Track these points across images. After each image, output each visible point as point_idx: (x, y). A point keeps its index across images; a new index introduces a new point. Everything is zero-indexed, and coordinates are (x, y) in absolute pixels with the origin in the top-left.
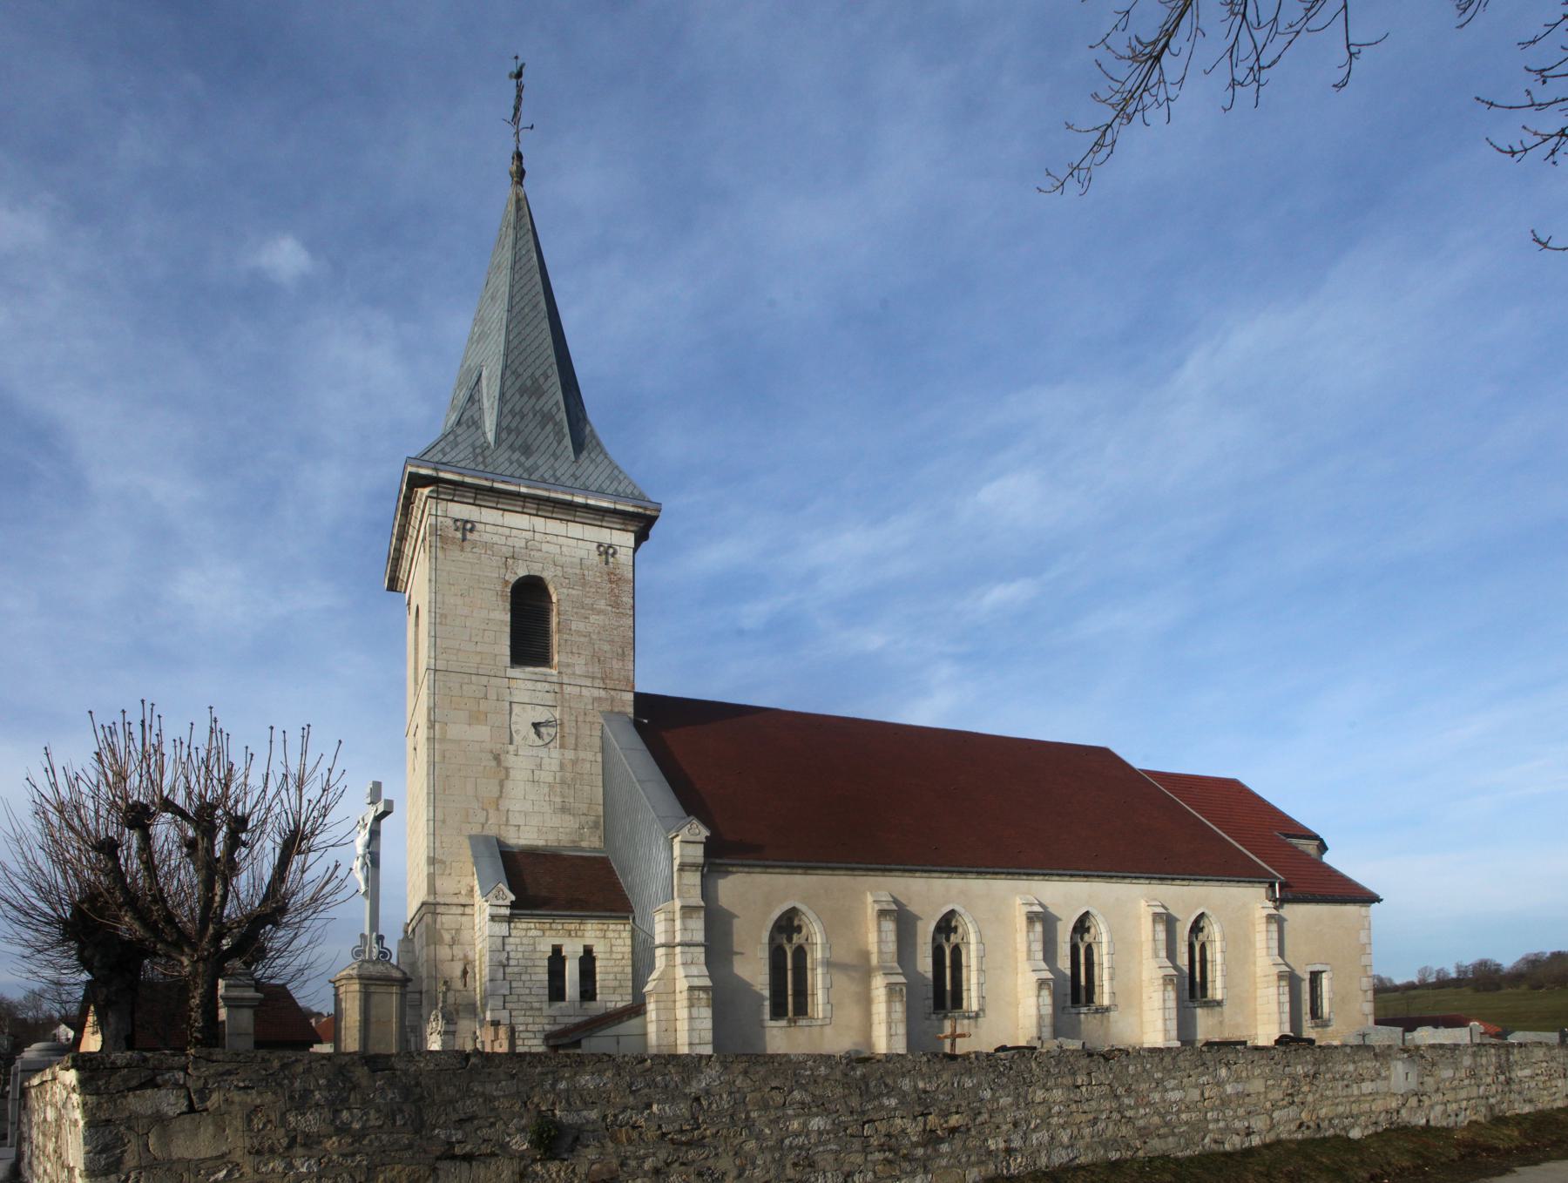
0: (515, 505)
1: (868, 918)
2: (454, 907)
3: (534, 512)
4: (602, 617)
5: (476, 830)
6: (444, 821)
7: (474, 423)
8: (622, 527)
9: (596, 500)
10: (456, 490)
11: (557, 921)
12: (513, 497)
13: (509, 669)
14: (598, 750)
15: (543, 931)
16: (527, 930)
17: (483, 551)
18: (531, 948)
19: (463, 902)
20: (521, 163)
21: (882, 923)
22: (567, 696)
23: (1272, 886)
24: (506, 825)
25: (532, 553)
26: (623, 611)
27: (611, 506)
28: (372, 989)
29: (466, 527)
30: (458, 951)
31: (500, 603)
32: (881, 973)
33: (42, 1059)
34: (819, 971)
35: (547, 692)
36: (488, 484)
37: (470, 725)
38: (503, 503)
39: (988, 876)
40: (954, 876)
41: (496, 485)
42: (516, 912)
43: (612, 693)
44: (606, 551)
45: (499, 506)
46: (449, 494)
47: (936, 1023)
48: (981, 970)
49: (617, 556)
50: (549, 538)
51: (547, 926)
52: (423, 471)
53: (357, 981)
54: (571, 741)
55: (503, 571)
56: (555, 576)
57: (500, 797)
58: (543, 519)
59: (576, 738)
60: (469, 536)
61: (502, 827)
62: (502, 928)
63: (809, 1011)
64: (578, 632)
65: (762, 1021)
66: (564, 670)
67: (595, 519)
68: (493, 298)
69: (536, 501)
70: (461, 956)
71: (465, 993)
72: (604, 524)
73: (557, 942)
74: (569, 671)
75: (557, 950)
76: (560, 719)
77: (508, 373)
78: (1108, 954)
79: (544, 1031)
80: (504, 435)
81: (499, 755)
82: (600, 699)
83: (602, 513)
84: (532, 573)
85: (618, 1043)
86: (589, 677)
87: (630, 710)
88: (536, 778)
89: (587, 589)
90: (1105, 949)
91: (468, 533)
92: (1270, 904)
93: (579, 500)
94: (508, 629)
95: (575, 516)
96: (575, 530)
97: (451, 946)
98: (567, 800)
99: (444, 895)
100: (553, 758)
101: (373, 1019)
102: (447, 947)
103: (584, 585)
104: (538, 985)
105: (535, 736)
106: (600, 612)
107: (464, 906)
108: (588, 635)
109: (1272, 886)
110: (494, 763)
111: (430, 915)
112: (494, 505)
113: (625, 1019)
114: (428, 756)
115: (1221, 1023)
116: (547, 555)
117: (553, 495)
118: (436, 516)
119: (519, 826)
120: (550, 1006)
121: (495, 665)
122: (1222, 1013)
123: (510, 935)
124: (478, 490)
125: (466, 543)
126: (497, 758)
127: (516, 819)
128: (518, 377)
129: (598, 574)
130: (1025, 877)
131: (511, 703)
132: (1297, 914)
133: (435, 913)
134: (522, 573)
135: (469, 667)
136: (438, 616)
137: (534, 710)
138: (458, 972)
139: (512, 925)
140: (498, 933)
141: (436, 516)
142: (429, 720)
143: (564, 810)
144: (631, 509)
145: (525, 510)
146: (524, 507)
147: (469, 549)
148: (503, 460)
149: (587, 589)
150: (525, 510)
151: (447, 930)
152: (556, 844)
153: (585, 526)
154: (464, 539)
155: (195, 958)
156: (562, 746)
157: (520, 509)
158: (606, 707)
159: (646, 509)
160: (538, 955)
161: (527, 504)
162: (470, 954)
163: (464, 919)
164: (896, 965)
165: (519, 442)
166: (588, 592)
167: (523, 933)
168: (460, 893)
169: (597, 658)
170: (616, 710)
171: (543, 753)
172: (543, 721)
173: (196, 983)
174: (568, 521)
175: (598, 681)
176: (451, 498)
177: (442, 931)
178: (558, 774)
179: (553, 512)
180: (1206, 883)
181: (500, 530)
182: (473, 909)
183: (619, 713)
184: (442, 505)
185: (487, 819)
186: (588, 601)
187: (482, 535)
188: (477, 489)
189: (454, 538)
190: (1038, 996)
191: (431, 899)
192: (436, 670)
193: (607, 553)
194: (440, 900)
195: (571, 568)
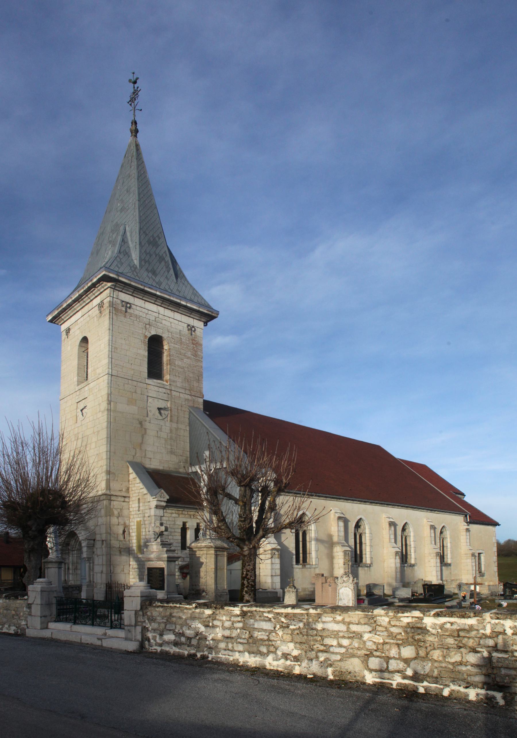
0: (152, 299)
1: (331, 520)
2: (120, 497)
3: (160, 304)
4: (190, 360)
5: (130, 459)
6: (115, 453)
7: (127, 253)
8: (199, 318)
9: (191, 304)
10: (125, 287)
11: (185, 510)
12: (152, 296)
13: (147, 379)
14: (187, 424)
15: (179, 514)
16: (171, 513)
17: (135, 319)
18: (173, 523)
19: (124, 495)
20: (137, 126)
21: (339, 522)
22: (173, 396)
23: (466, 516)
24: (145, 457)
25: (158, 324)
26: (198, 359)
27: (197, 308)
28: (218, 553)
29: (127, 306)
30: (121, 520)
31: (143, 346)
32: (340, 545)
33: (145, 591)
34: (313, 543)
35: (164, 393)
36: (142, 287)
37: (128, 405)
38: (146, 298)
39: (373, 504)
40: (362, 503)
41: (146, 289)
42: (169, 504)
43: (194, 397)
44: (191, 329)
45: (144, 298)
46: (121, 288)
47: (356, 568)
48: (371, 546)
49: (196, 332)
50: (165, 318)
51: (181, 512)
52: (112, 275)
53: (213, 549)
54: (175, 418)
55: (144, 330)
56: (168, 337)
57: (142, 443)
58: (163, 308)
59: (178, 418)
60: (128, 310)
61: (143, 458)
62: (160, 512)
63: (307, 561)
64: (178, 366)
65: (292, 565)
66: (172, 383)
67: (187, 313)
68: (128, 191)
69: (162, 300)
70: (123, 523)
71: (124, 542)
72: (191, 316)
73: (185, 520)
74: (174, 384)
75: (184, 524)
76: (170, 407)
77: (142, 232)
78: (413, 541)
79: (179, 565)
80: (143, 263)
81: (142, 422)
82: (188, 400)
83: (192, 311)
84: (158, 334)
85: (231, 573)
86: (183, 388)
87: (202, 407)
88: (159, 436)
89: (183, 346)
90: (412, 539)
91: (128, 309)
92: (466, 524)
93: (183, 303)
94: (147, 360)
95: (179, 310)
96: (178, 316)
97: (118, 517)
98: (173, 448)
99: (114, 491)
100: (167, 426)
101: (218, 568)
102: (116, 518)
103: (181, 343)
104: (176, 542)
105: (159, 415)
106: (188, 358)
107: (125, 497)
108: (183, 368)
109: (466, 516)
110: (139, 426)
111: (108, 500)
112: (141, 297)
113: (234, 561)
114: (107, 418)
115: (450, 573)
116: (164, 326)
117: (172, 298)
118: (113, 297)
119: (151, 458)
120: (181, 552)
121: (140, 376)
122: (451, 569)
123: (164, 516)
124: (136, 289)
125: (127, 314)
126: (141, 423)
127: (150, 455)
128: (147, 235)
129: (188, 339)
130: (386, 506)
131: (147, 396)
132: (474, 527)
133: (110, 500)
134: (153, 333)
135: (128, 376)
136: (113, 348)
137: (158, 401)
138: (121, 532)
139: (165, 511)
140: (158, 515)
141: (113, 297)
142: (108, 400)
143: (172, 452)
144: (206, 312)
145: (156, 303)
146: (155, 301)
147: (128, 317)
148: (144, 275)
149: (183, 346)
150: (156, 303)
151: (116, 509)
152: (168, 469)
153: (182, 315)
154: (126, 312)
155: (251, 547)
156: (171, 421)
157: (153, 302)
158: (191, 404)
159: (212, 313)
160: (177, 526)
161: (157, 300)
162: (127, 522)
163: (124, 504)
164: (344, 542)
165: (150, 269)
166: (183, 347)
167: (170, 515)
168: (122, 490)
169: (187, 380)
170: (195, 406)
171: (162, 423)
172: (163, 407)
173: (251, 559)
174: (175, 311)
175: (188, 391)
176: (121, 290)
177: (114, 510)
178: (169, 435)
179: (169, 306)
180: (445, 513)
181: (144, 310)
182: (129, 499)
183: (197, 408)
184: (116, 292)
185: (136, 454)
186: (183, 351)
187: (134, 311)
188: (135, 288)
189: (121, 310)
190: (395, 559)
191: (108, 492)
192: (112, 375)
193: (191, 330)
194: (112, 493)
195: (176, 334)
